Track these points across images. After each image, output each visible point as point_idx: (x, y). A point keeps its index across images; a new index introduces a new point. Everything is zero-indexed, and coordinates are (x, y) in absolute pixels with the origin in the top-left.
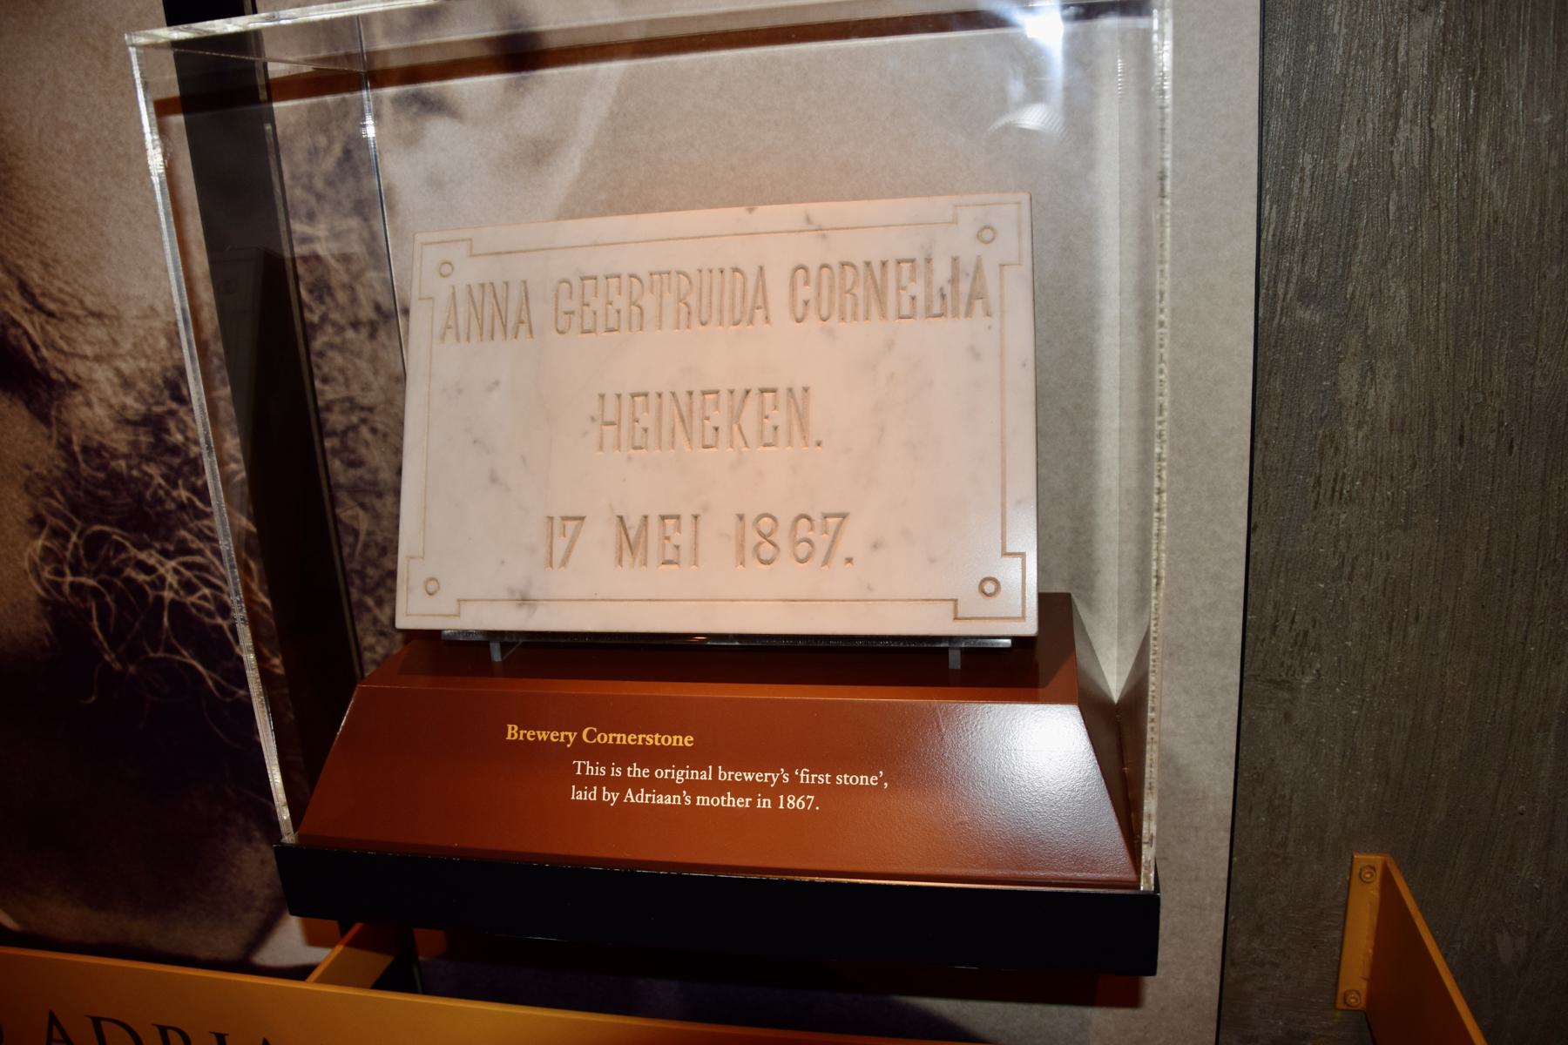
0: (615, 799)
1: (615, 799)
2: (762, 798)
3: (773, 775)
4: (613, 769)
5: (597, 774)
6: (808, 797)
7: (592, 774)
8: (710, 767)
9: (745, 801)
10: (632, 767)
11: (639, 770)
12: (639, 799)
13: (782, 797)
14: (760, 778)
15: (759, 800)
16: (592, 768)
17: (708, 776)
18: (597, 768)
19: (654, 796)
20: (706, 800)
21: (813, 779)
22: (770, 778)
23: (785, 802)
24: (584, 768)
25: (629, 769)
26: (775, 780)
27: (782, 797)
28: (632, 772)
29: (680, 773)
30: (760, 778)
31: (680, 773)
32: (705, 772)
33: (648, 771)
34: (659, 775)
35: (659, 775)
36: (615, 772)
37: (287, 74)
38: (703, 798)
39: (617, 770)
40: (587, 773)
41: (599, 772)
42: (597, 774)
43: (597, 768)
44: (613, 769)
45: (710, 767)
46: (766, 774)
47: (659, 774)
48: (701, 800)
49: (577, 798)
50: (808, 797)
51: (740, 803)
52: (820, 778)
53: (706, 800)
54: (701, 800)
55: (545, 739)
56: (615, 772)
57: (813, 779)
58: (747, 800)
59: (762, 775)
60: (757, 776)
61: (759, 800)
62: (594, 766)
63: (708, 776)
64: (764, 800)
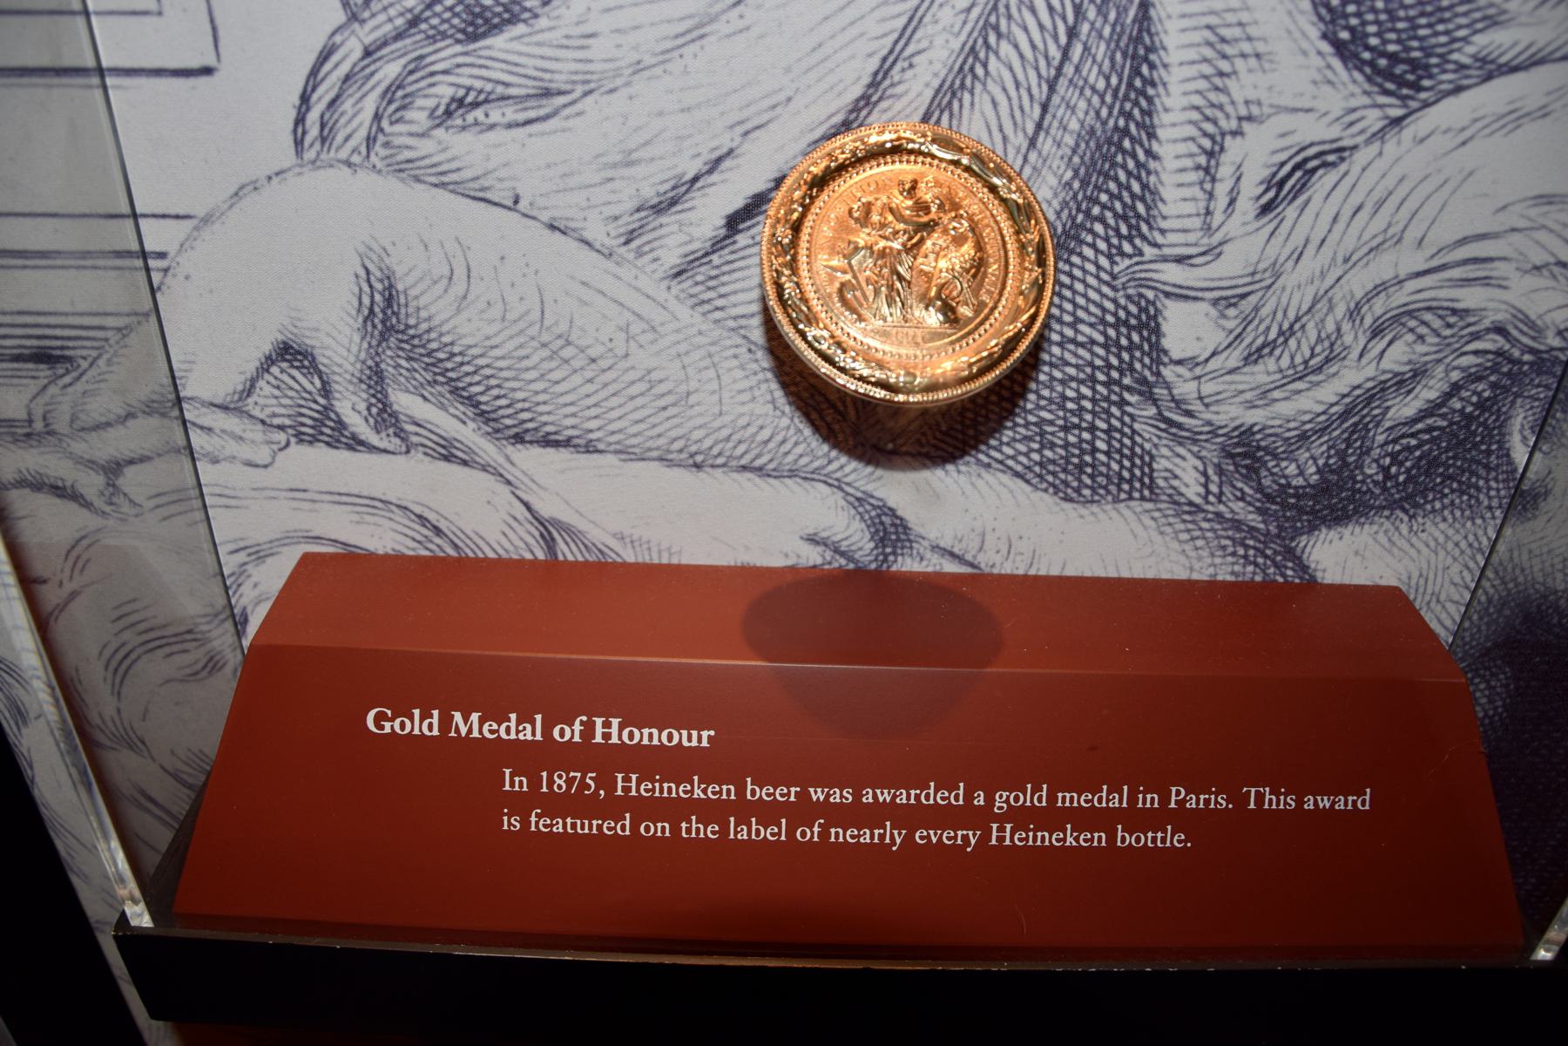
0: (898, 841)
1: (898, 841)
2: (1145, 793)
3: (971, 833)
4: (505, 818)
5: (1282, 807)
6: (572, 774)
7: (1274, 807)
8: (784, 821)
9: (789, 792)
10: (689, 822)
11: (701, 826)
12: (1100, 801)
13: (544, 774)
14: (949, 838)
15: (1140, 796)
16: (1274, 797)
17: (1121, 801)
18: (1282, 798)
19: (1213, 797)
20: (1072, 798)
21: (1350, 803)
22: (965, 838)
23: (551, 782)
24: (1260, 798)
25: (684, 825)
26: (973, 842)
27: (544, 774)
28: (689, 831)
29: (1001, 797)
30: (949, 838)
31: (1001, 797)
32: (745, 828)
33: (717, 828)
34: (670, 734)
35: (670, 734)
36: (1286, 803)
37: (38, 801)
38: (1068, 795)
39: (1288, 800)
40: (1266, 807)
41: (1286, 803)
42: (1282, 807)
43: (1282, 798)
44: (505, 818)
45: (784, 821)
46: (960, 833)
47: (647, 829)
48: (1064, 797)
49: (1111, 805)
50: (572, 774)
51: (646, 791)
52: (1224, 803)
53: (1072, 798)
54: (1064, 797)
55: (888, 800)
56: (510, 824)
57: (1350, 803)
58: (793, 790)
59: (952, 834)
60: (945, 834)
61: (1140, 796)
62: (1278, 795)
63: (1121, 801)
64: (1149, 796)
